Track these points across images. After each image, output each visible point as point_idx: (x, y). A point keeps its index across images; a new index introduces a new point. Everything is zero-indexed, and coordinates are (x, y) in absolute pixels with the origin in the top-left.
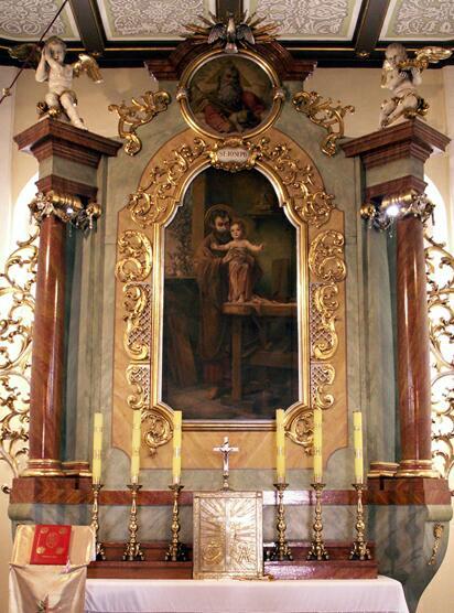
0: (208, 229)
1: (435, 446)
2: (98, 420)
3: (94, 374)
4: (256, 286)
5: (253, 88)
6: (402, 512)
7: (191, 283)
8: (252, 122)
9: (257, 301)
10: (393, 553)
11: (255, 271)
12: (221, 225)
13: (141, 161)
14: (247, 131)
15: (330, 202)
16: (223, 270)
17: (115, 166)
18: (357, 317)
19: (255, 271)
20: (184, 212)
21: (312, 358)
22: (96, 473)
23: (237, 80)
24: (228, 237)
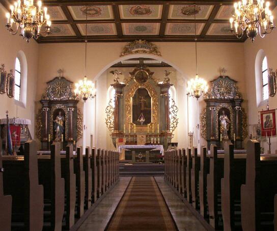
0: (138, 98)
1: (171, 128)
2: (125, 125)
3: (123, 119)
4: (145, 106)
5: (145, 76)
6: (165, 137)
7: (136, 106)
8: (145, 81)
9: (146, 108)
10: (163, 143)
11: (145, 104)
12: (154, 139)
13: (128, 88)
14: (135, 15)
15: (156, 94)
16: (141, 104)
17: (125, 88)
18: (159, 110)
19: (145, 104)
20: (135, 95)
21: (153, 116)
22: (232, 97)
23: (142, 75)
24: (141, 99)
